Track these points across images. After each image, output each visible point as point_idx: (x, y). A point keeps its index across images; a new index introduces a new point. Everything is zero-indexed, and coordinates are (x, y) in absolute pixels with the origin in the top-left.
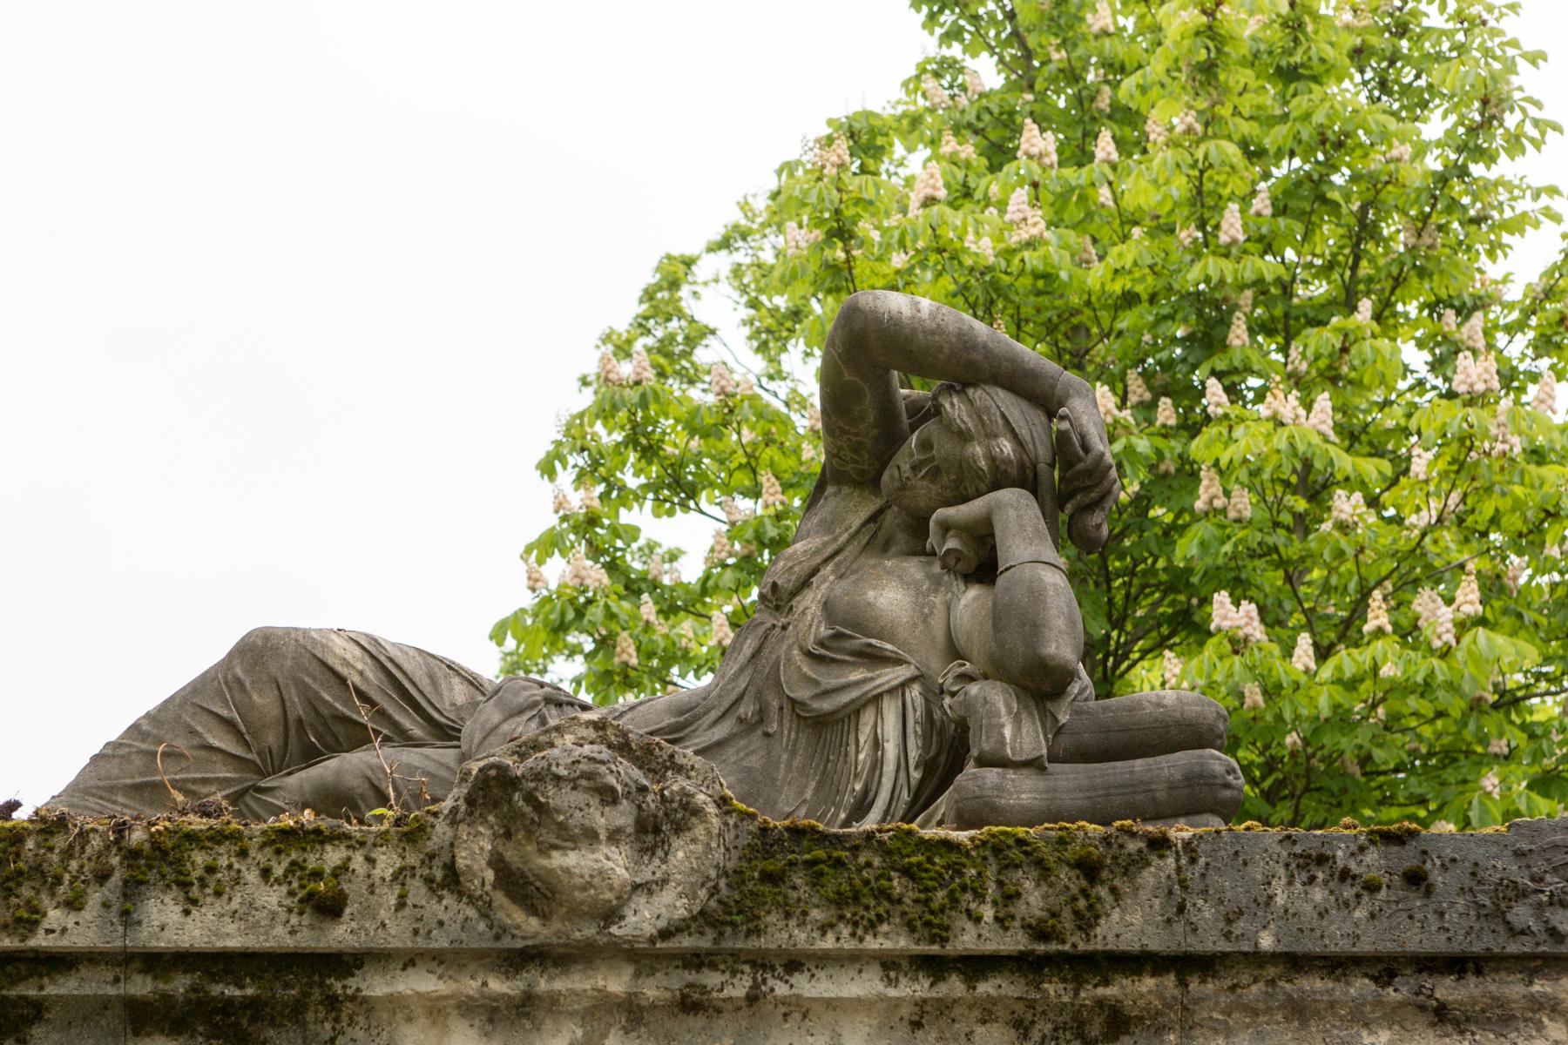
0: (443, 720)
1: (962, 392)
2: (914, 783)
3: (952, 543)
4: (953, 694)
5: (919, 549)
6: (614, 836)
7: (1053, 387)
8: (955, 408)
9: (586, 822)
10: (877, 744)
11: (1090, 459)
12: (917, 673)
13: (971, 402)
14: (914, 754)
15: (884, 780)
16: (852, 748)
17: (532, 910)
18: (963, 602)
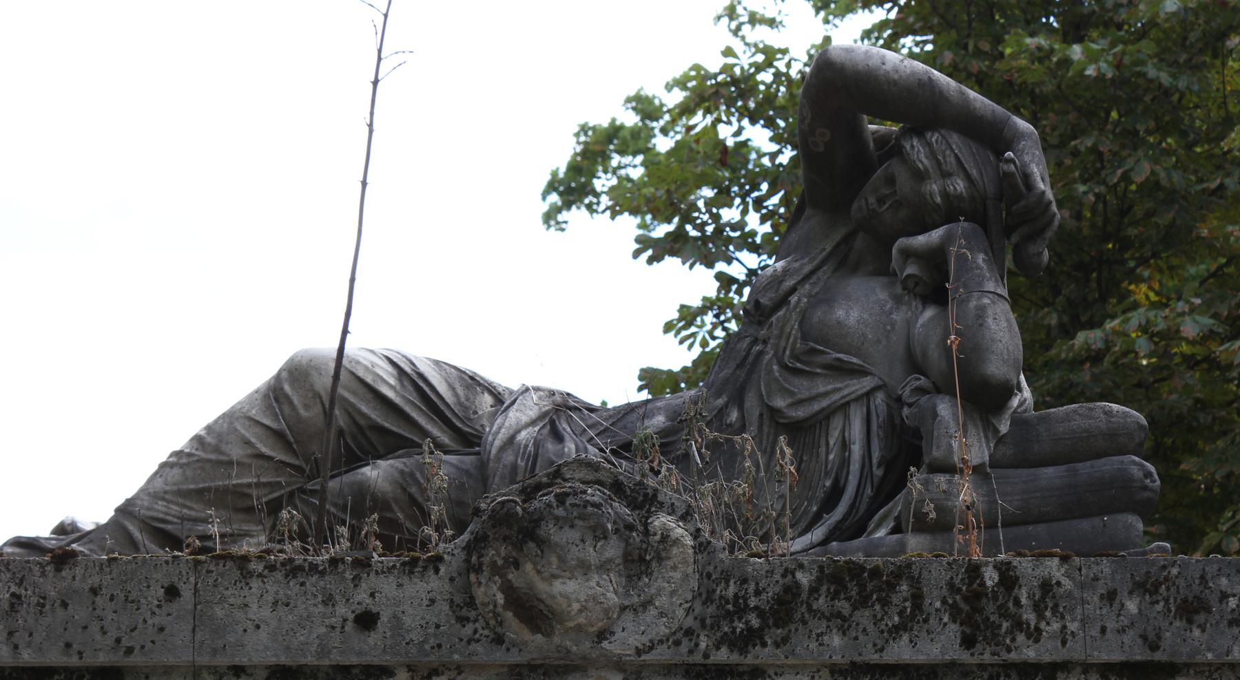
2: (876, 480)
3: (911, 270)
4: (910, 405)
5: (883, 270)
6: (603, 567)
8: (916, 150)
9: (581, 555)
10: (845, 445)
12: (881, 383)
13: (929, 145)
15: (850, 477)
16: (823, 449)
17: (535, 629)
18: (920, 322)
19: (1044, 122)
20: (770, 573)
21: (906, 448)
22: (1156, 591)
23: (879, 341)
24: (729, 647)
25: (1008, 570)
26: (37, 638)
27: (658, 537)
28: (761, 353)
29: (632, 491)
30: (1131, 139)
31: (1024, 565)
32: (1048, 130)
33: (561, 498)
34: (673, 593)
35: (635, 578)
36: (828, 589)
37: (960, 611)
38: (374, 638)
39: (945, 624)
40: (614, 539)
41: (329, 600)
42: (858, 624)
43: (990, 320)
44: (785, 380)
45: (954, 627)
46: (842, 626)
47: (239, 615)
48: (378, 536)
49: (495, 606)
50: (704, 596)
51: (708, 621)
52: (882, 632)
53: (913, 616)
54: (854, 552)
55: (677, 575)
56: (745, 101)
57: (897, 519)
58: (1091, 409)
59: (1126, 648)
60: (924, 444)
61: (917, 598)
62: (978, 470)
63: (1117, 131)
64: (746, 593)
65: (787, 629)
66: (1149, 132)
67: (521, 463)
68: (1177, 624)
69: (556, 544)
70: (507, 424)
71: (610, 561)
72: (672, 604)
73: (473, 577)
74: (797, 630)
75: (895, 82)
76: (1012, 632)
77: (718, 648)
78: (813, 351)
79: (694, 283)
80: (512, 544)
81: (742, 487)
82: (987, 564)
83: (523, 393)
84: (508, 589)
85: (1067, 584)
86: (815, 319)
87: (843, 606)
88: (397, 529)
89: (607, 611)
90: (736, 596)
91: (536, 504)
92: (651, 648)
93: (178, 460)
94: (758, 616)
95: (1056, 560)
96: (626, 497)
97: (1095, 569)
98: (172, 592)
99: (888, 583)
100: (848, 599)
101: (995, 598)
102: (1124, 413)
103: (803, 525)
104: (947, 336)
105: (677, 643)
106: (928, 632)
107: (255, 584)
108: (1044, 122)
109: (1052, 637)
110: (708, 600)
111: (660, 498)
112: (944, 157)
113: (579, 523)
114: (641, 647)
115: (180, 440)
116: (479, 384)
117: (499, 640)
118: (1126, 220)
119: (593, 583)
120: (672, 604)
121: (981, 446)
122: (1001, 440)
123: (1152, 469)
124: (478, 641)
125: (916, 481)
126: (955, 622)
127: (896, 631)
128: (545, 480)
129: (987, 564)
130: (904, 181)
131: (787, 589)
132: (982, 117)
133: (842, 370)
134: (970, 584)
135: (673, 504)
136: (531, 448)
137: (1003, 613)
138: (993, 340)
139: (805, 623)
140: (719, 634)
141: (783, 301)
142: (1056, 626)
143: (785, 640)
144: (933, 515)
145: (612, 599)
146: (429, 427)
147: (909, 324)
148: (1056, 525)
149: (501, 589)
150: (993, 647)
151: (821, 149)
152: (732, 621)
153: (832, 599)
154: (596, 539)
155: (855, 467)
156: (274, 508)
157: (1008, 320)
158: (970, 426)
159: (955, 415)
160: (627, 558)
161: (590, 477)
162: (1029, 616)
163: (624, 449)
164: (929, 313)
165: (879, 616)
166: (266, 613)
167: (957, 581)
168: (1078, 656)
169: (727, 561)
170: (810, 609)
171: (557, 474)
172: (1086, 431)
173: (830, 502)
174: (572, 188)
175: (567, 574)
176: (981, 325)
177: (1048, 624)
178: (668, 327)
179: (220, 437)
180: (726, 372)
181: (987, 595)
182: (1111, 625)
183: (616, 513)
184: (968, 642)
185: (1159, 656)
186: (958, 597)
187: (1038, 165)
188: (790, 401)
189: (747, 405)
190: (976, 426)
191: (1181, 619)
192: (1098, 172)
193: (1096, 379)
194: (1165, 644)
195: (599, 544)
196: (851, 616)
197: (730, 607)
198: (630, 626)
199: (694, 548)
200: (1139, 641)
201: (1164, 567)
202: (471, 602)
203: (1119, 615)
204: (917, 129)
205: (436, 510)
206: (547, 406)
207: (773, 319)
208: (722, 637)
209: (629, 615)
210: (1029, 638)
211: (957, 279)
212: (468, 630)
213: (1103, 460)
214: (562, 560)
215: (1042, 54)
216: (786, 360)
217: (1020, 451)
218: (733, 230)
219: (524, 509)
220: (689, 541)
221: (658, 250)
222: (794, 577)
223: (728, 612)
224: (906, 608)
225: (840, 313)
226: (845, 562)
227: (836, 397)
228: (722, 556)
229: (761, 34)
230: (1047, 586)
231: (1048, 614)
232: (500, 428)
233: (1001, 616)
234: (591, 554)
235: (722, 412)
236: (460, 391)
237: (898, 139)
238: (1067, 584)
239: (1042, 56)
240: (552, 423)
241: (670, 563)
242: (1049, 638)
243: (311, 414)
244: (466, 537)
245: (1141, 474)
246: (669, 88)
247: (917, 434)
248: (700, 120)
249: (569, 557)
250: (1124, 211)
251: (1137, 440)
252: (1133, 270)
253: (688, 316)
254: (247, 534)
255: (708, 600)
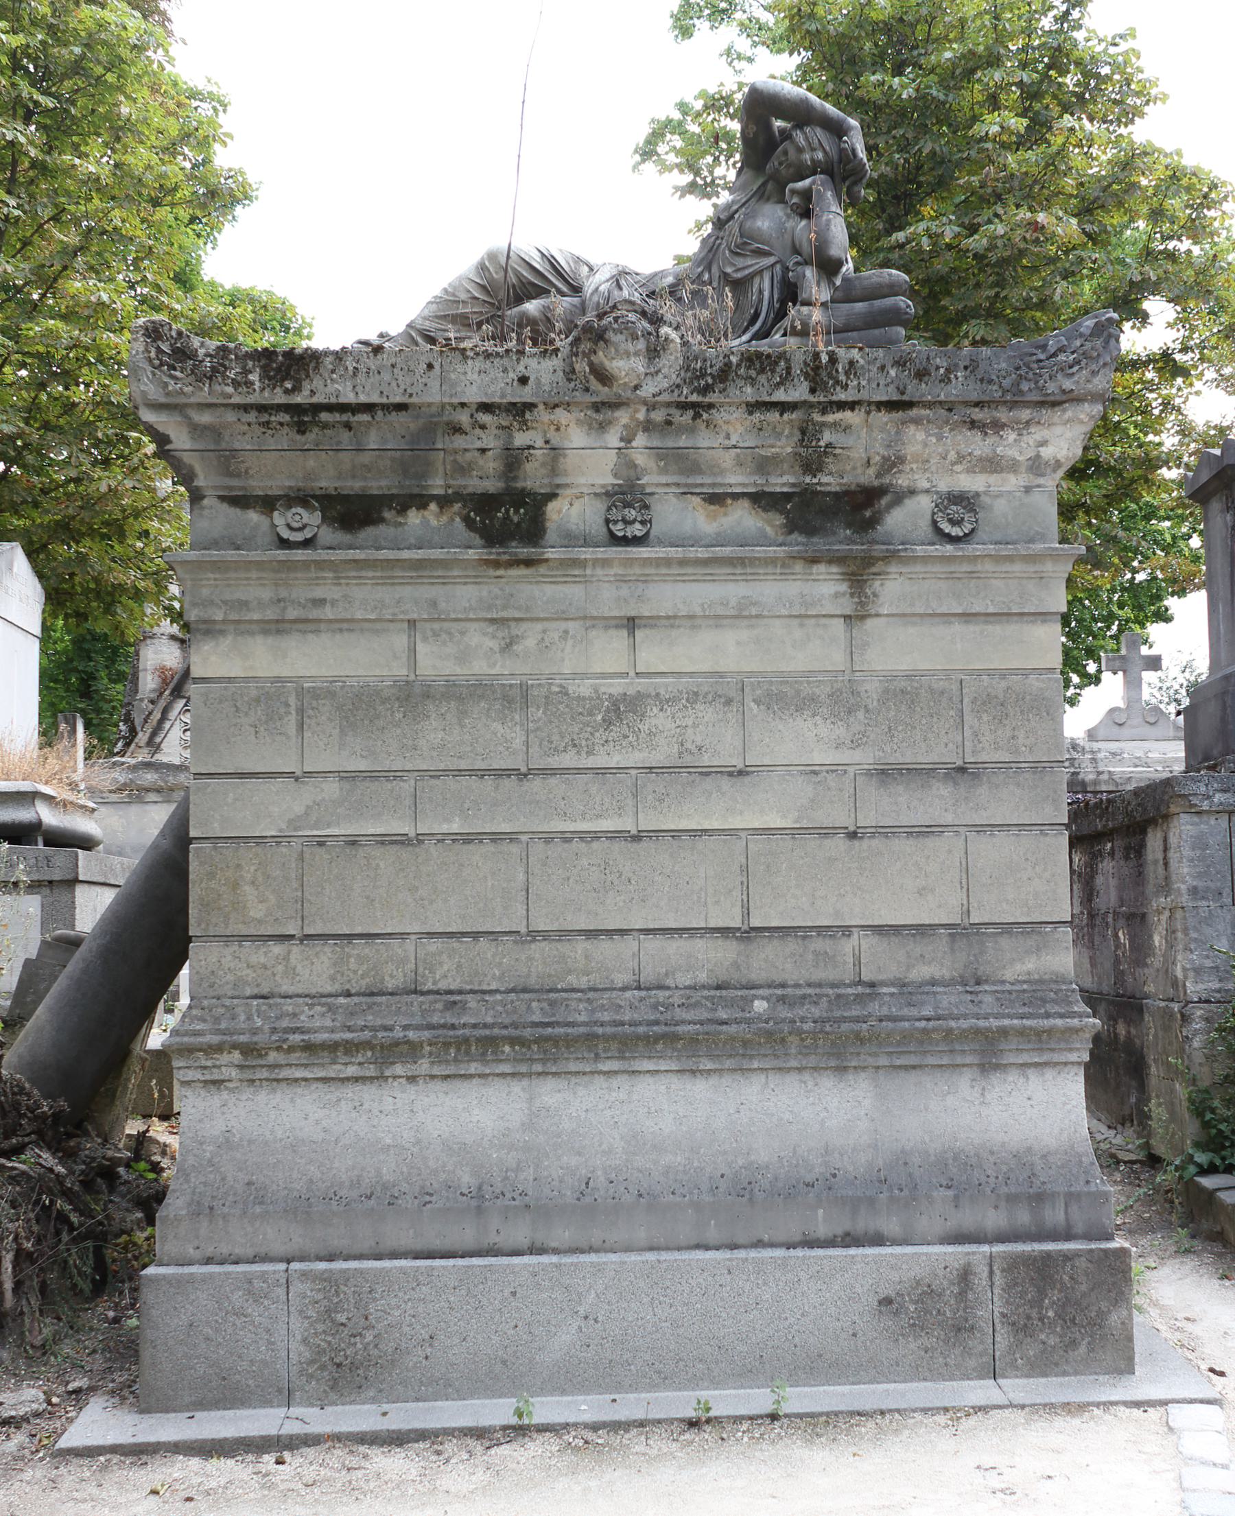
1: (801, 128)
3: (795, 200)
5: (782, 200)
6: (637, 354)
8: (799, 137)
10: (761, 292)
14: (776, 297)
17: (604, 384)
20: (717, 356)
21: (790, 293)
26: (367, 389)
30: (923, 129)
31: (841, 352)
33: (616, 319)
38: (528, 389)
40: (642, 339)
41: (505, 370)
45: (806, 383)
47: (462, 377)
48: (531, 339)
54: (763, 346)
61: (788, 369)
62: (824, 304)
66: (933, 124)
78: (746, 243)
84: (591, 364)
85: (862, 362)
88: (538, 333)
91: (604, 322)
93: (437, 301)
98: (430, 366)
107: (470, 362)
109: (853, 388)
110: (688, 370)
115: (437, 291)
117: (587, 390)
122: (836, 289)
127: (778, 385)
130: (792, 154)
131: (726, 365)
133: (760, 253)
137: (830, 376)
141: (731, 217)
142: (855, 383)
143: (724, 390)
146: (557, 283)
147: (793, 230)
148: (863, 332)
154: (633, 339)
155: (765, 303)
156: (479, 325)
158: (822, 285)
160: (648, 350)
162: (842, 378)
163: (652, 295)
164: (804, 222)
166: (475, 376)
168: (866, 397)
171: (614, 307)
174: (647, 152)
178: (690, 232)
179: (455, 288)
182: (882, 382)
184: (813, 391)
185: (905, 398)
192: (905, 147)
193: (901, 257)
194: (907, 392)
202: (573, 371)
204: (799, 126)
205: (559, 325)
206: (614, 272)
209: (649, 377)
212: (573, 384)
214: (617, 350)
217: (847, 295)
220: (678, 340)
235: (700, 275)
238: (862, 362)
243: (498, 276)
244: (570, 338)
246: (696, 98)
247: (795, 285)
250: (919, 168)
254: (470, 338)
255: (688, 370)
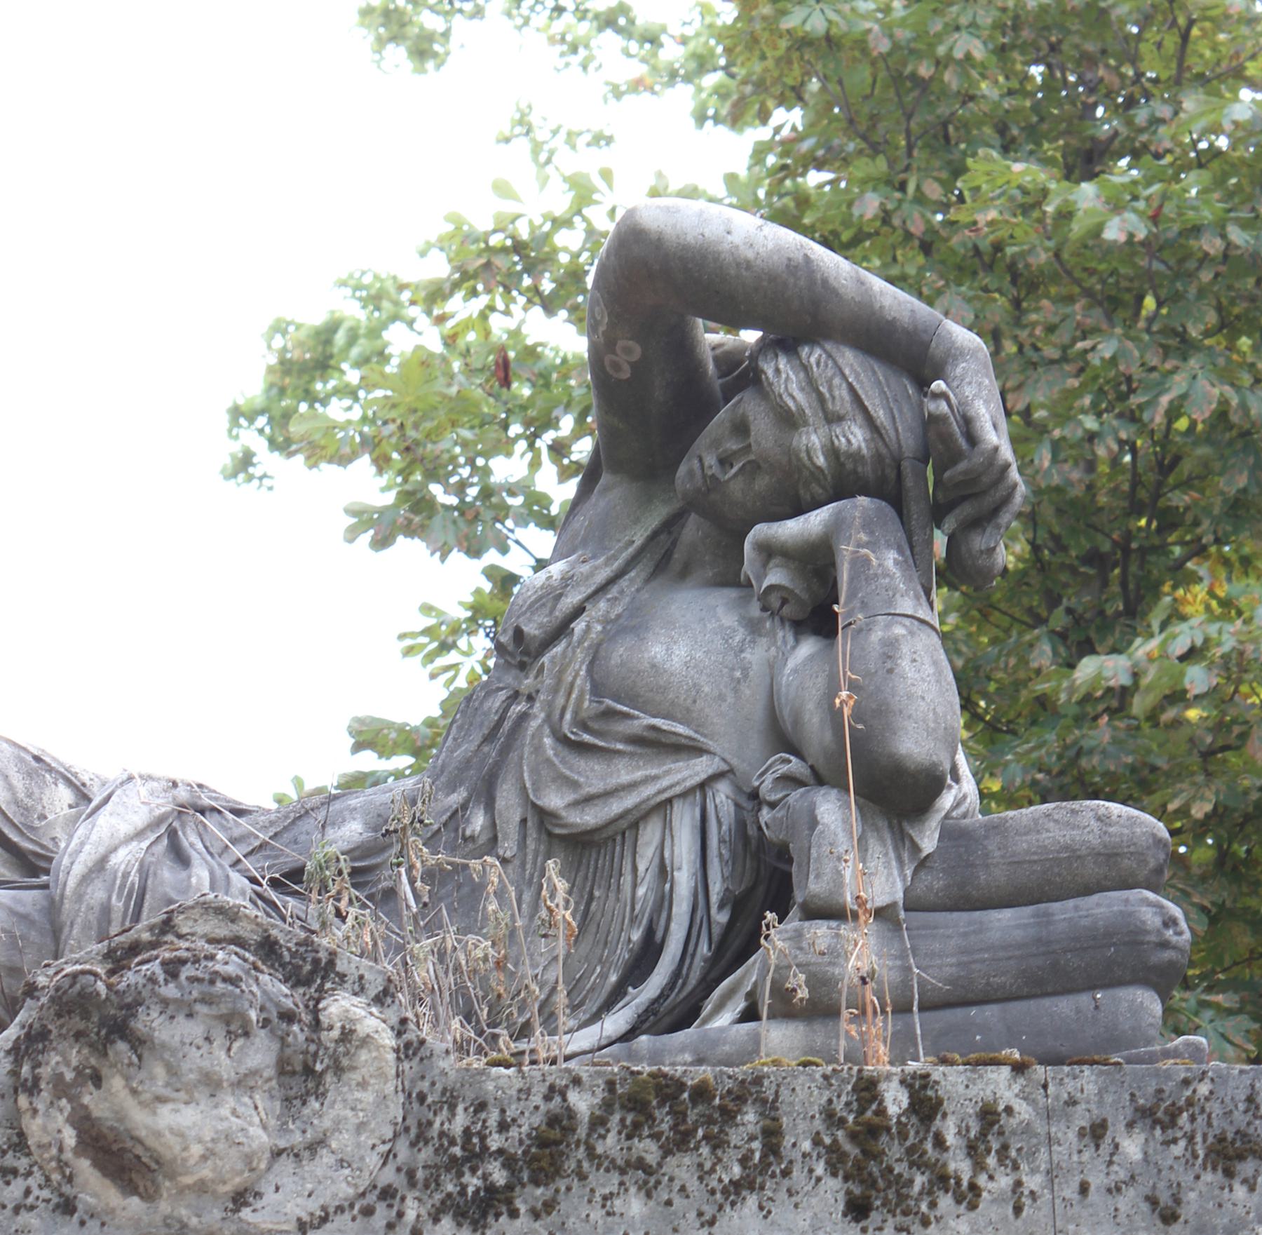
0: (31, 846)
2: (716, 931)
3: (776, 576)
4: (773, 805)
5: (729, 577)
6: (243, 1083)
7: (927, 345)
8: (784, 376)
9: (206, 1064)
10: (664, 872)
11: (978, 460)
12: (725, 767)
13: (806, 368)
15: (673, 926)
16: (627, 879)
17: (130, 1188)
18: (791, 664)
19: (1034, 317)
20: (525, 1092)
21: (766, 881)
22: (1173, 1123)
23: (721, 698)
24: (455, 1216)
25: (924, 1087)
27: (335, 1033)
28: (524, 717)
29: (294, 955)
31: (953, 1082)
32: (1038, 331)
33: (172, 969)
34: (361, 1127)
35: (297, 1102)
36: (623, 1120)
37: (843, 1156)
39: (819, 1180)
40: (261, 1038)
42: (671, 1179)
43: (905, 664)
44: (563, 762)
46: (646, 1182)
49: (61, 1150)
50: (413, 1131)
51: (420, 1174)
52: (713, 1192)
53: (764, 1165)
54: (676, 1054)
55: (368, 1097)
56: (537, 277)
57: (752, 997)
58: (1073, 812)
59: (1122, 1218)
60: (794, 869)
61: (772, 1135)
62: (883, 914)
63: (1155, 328)
64: (484, 1127)
65: (552, 1187)
67: (117, 904)
68: (1208, 1177)
69: (163, 1046)
70: (94, 837)
71: (254, 1073)
72: (358, 1145)
73: (23, 1101)
74: (569, 1189)
75: (748, 265)
76: (930, 1193)
77: (436, 1220)
78: (609, 714)
79: (458, 580)
80: (91, 1045)
81: (482, 947)
82: (888, 1077)
83: (122, 784)
84: (84, 1123)
85: (1024, 1111)
86: (615, 660)
87: (648, 1149)
89: (248, 1159)
90: (467, 1132)
92: (324, 1220)
94: (504, 1166)
95: (1006, 1071)
96: (283, 965)
97: (1070, 1085)
99: (723, 1110)
100: (656, 1136)
101: (903, 1136)
102: (1129, 818)
103: (592, 1006)
104: (833, 691)
105: (368, 1212)
106: (790, 1193)
108: (1034, 317)
109: (998, 1200)
110: (420, 1139)
111: (341, 966)
112: (830, 389)
113: (201, 1009)
114: (306, 1218)
116: (50, 769)
118: (1171, 480)
119: (225, 1111)
120: (358, 1145)
121: (890, 874)
122: (923, 864)
123: (1176, 911)
124: (32, 1208)
125: (779, 938)
126: (834, 1175)
128: (146, 936)
129: (888, 1077)
131: (553, 1120)
132: (892, 323)
134: (861, 1112)
135: (361, 977)
136: (134, 878)
137: (916, 1159)
138: (910, 696)
139: (582, 1177)
140: (438, 1197)
141: (561, 630)
142: (1004, 1181)
143: (549, 1206)
144: (803, 993)
145: (259, 1138)
147: (773, 669)
149: (71, 1121)
150: (899, 1218)
151: (626, 374)
152: (460, 1174)
153: (629, 1137)
155: (681, 909)
157: (935, 663)
159: (846, 821)
160: (283, 1068)
161: (223, 931)
162: (960, 1165)
165: (708, 1166)
167: (839, 1106)
169: (452, 1075)
170: (591, 1153)
172: (1066, 848)
173: (641, 963)
175: (182, 1095)
176: (890, 671)
177: (991, 1178)
180: (467, 748)
181: (888, 1129)
182: (1097, 1180)
183: (265, 992)
186: (840, 1134)
187: (987, 402)
188: (571, 797)
189: (500, 804)
190: (882, 840)
191: (1214, 1169)
195: (236, 1045)
196: (660, 1165)
197: (457, 1151)
198: (288, 1182)
199: (397, 1051)
200: (1145, 1207)
201: (1186, 1082)
203: (1110, 1163)
204: (785, 341)
206: (163, 805)
207: (545, 659)
208: (443, 1202)
209: (286, 1163)
210: (959, 1202)
211: (852, 595)
213: (1095, 898)
214: (172, 1071)
215: (1029, 200)
216: (566, 728)
217: (957, 886)
218: (512, 494)
219: (109, 987)
220: (387, 1039)
221: (382, 529)
222: (565, 1100)
223: (454, 1159)
224: (752, 1151)
225: (656, 650)
226: (651, 1075)
227: (648, 791)
228: (443, 1064)
229: (571, 161)
230: (988, 1115)
231: (991, 1161)
232: (82, 844)
233: (912, 1164)
234: (222, 1062)
235: (457, 817)
236: (18, 782)
237: (754, 358)
238: (1024, 1111)
239: (1030, 202)
240: (172, 834)
241: (356, 1077)
242: (994, 1201)
245: (1157, 921)
247: (783, 853)
248: (460, 307)
249: (185, 1066)
251: (1152, 863)
252: (1180, 565)
253: (444, 640)
255: (420, 1139)
